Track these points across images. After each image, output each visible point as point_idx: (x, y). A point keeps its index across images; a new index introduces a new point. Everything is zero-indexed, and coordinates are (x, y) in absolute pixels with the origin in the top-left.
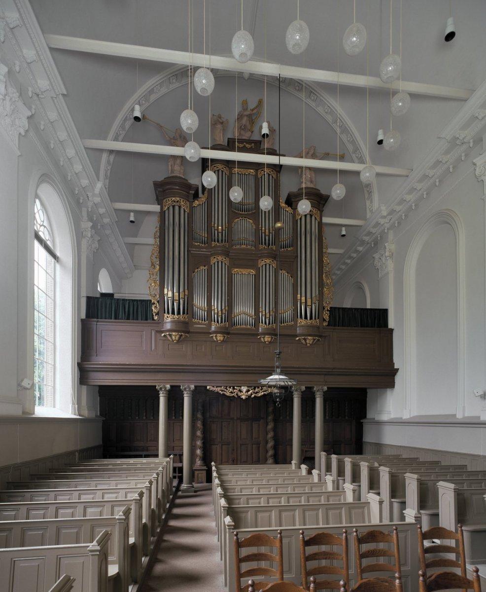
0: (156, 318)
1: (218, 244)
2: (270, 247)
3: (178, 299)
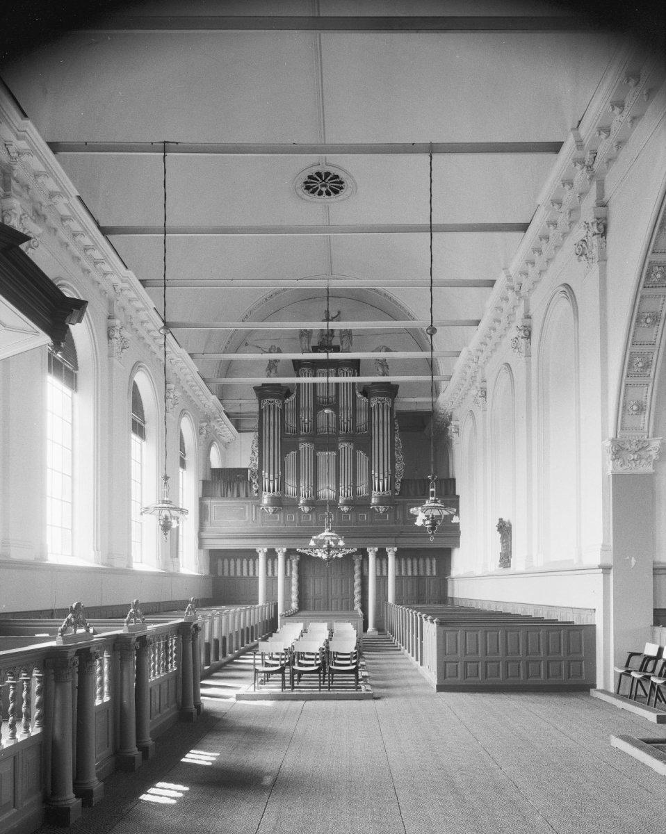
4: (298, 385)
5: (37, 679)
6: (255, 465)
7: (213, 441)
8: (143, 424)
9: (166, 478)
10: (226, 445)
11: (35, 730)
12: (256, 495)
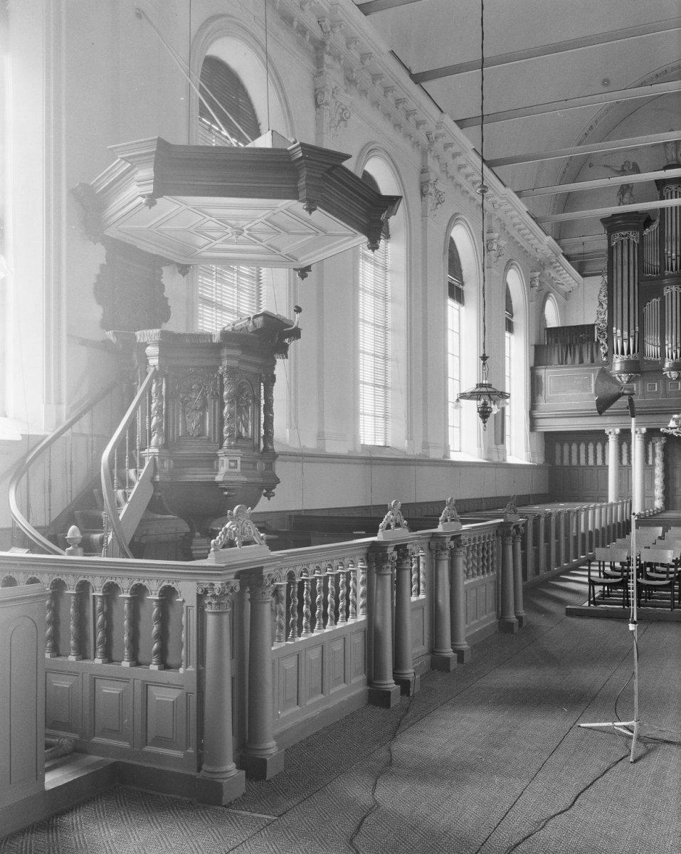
1: (672, 273)
4: (662, 210)
5: (361, 571)
6: (603, 321)
7: (549, 292)
8: (461, 286)
9: (484, 358)
10: (567, 295)
11: (362, 617)
12: (605, 359)
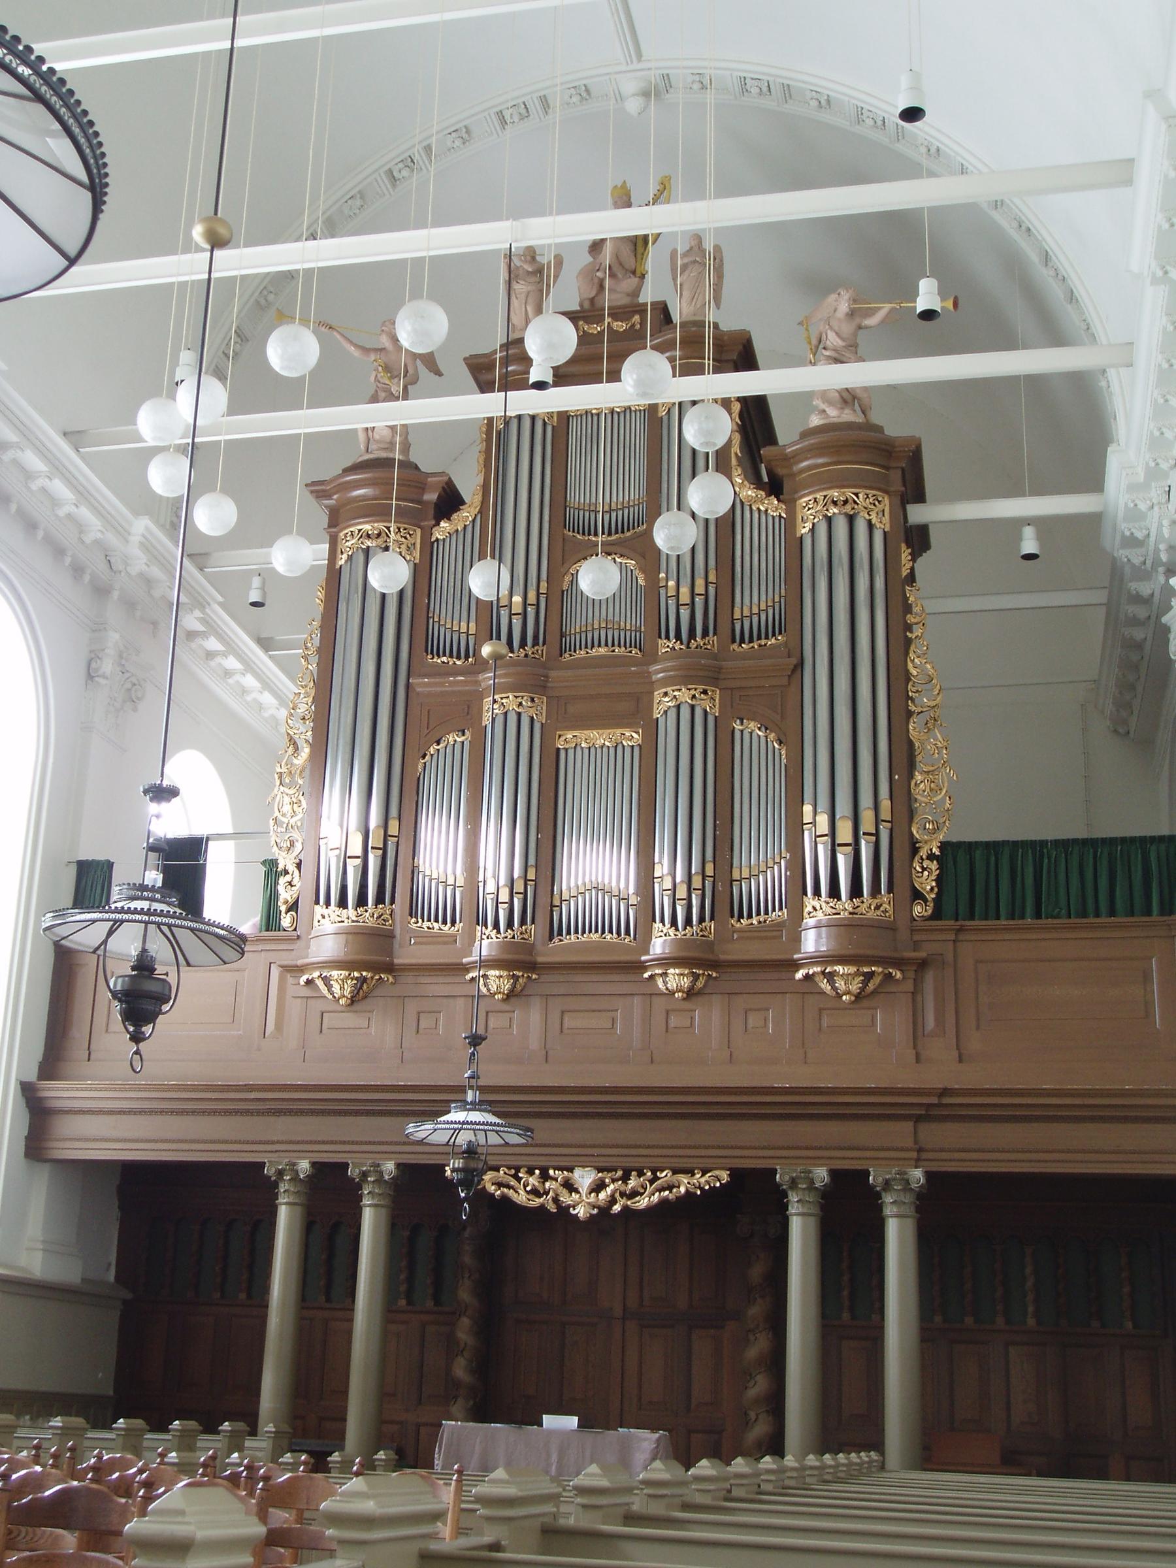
0: (286, 921)
2: (693, 644)
3: (849, 840)
